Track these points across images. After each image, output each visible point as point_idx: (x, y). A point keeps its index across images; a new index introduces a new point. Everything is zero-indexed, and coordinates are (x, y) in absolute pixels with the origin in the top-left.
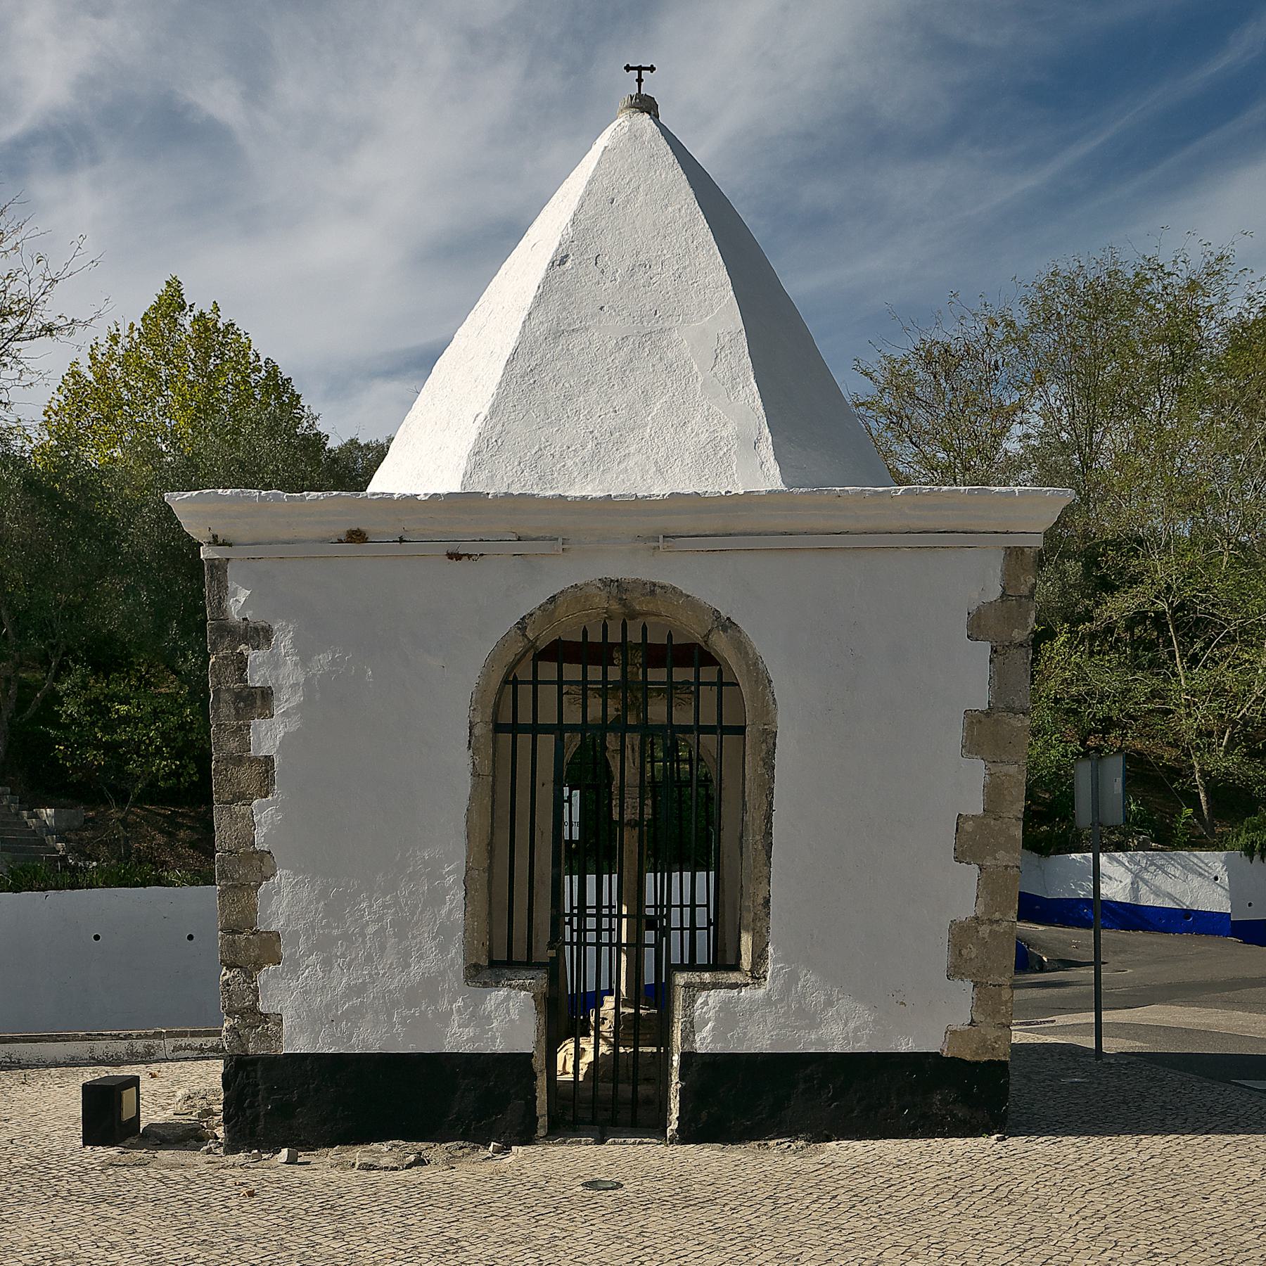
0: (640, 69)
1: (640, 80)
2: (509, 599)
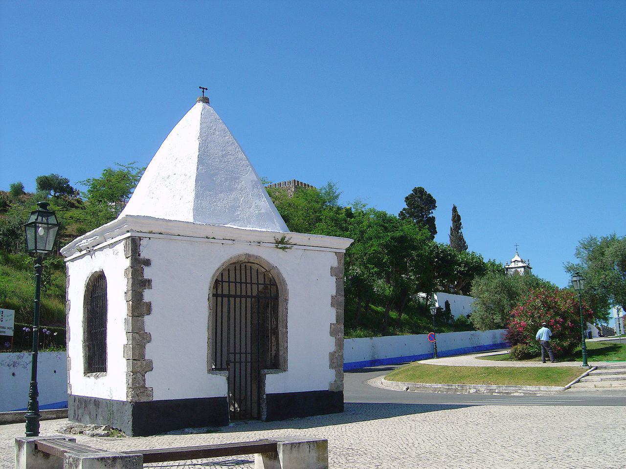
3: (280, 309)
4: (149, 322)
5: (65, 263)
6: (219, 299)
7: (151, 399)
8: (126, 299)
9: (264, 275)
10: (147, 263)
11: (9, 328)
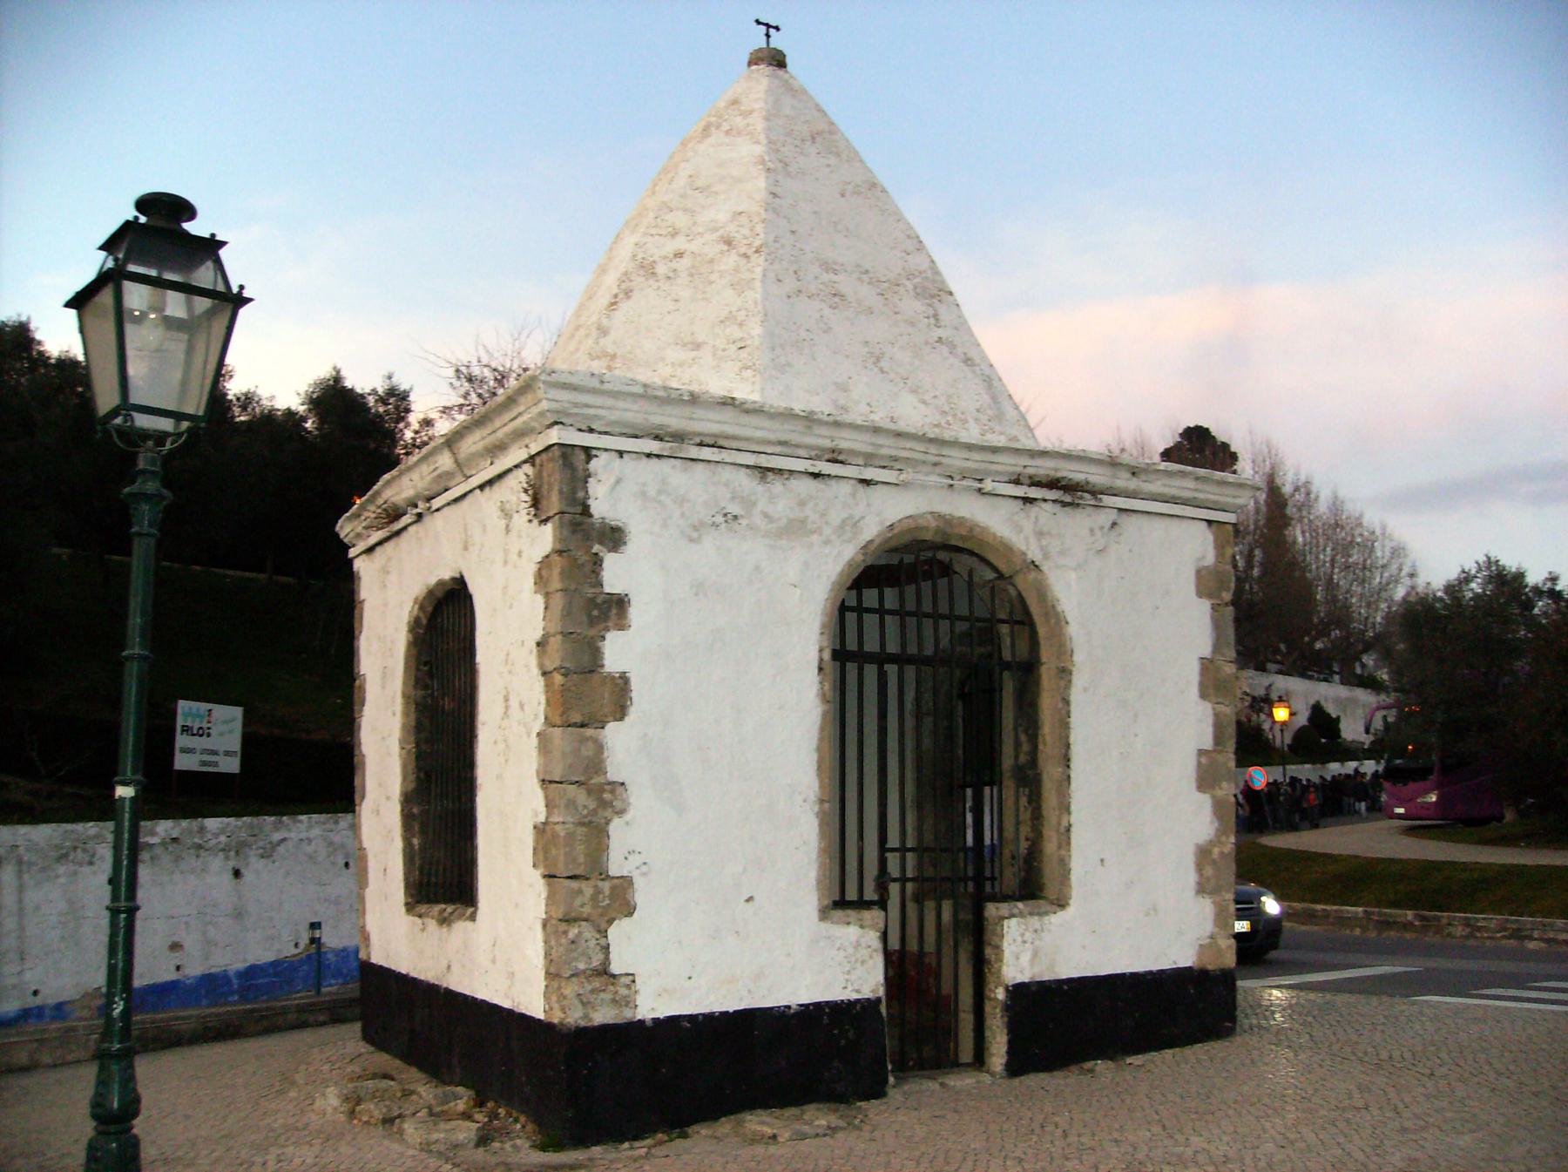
3: (1047, 702)
4: (620, 742)
5: (351, 560)
6: (852, 668)
7: (627, 1015)
8: (541, 666)
9: (993, 588)
10: (614, 537)
11: (227, 753)
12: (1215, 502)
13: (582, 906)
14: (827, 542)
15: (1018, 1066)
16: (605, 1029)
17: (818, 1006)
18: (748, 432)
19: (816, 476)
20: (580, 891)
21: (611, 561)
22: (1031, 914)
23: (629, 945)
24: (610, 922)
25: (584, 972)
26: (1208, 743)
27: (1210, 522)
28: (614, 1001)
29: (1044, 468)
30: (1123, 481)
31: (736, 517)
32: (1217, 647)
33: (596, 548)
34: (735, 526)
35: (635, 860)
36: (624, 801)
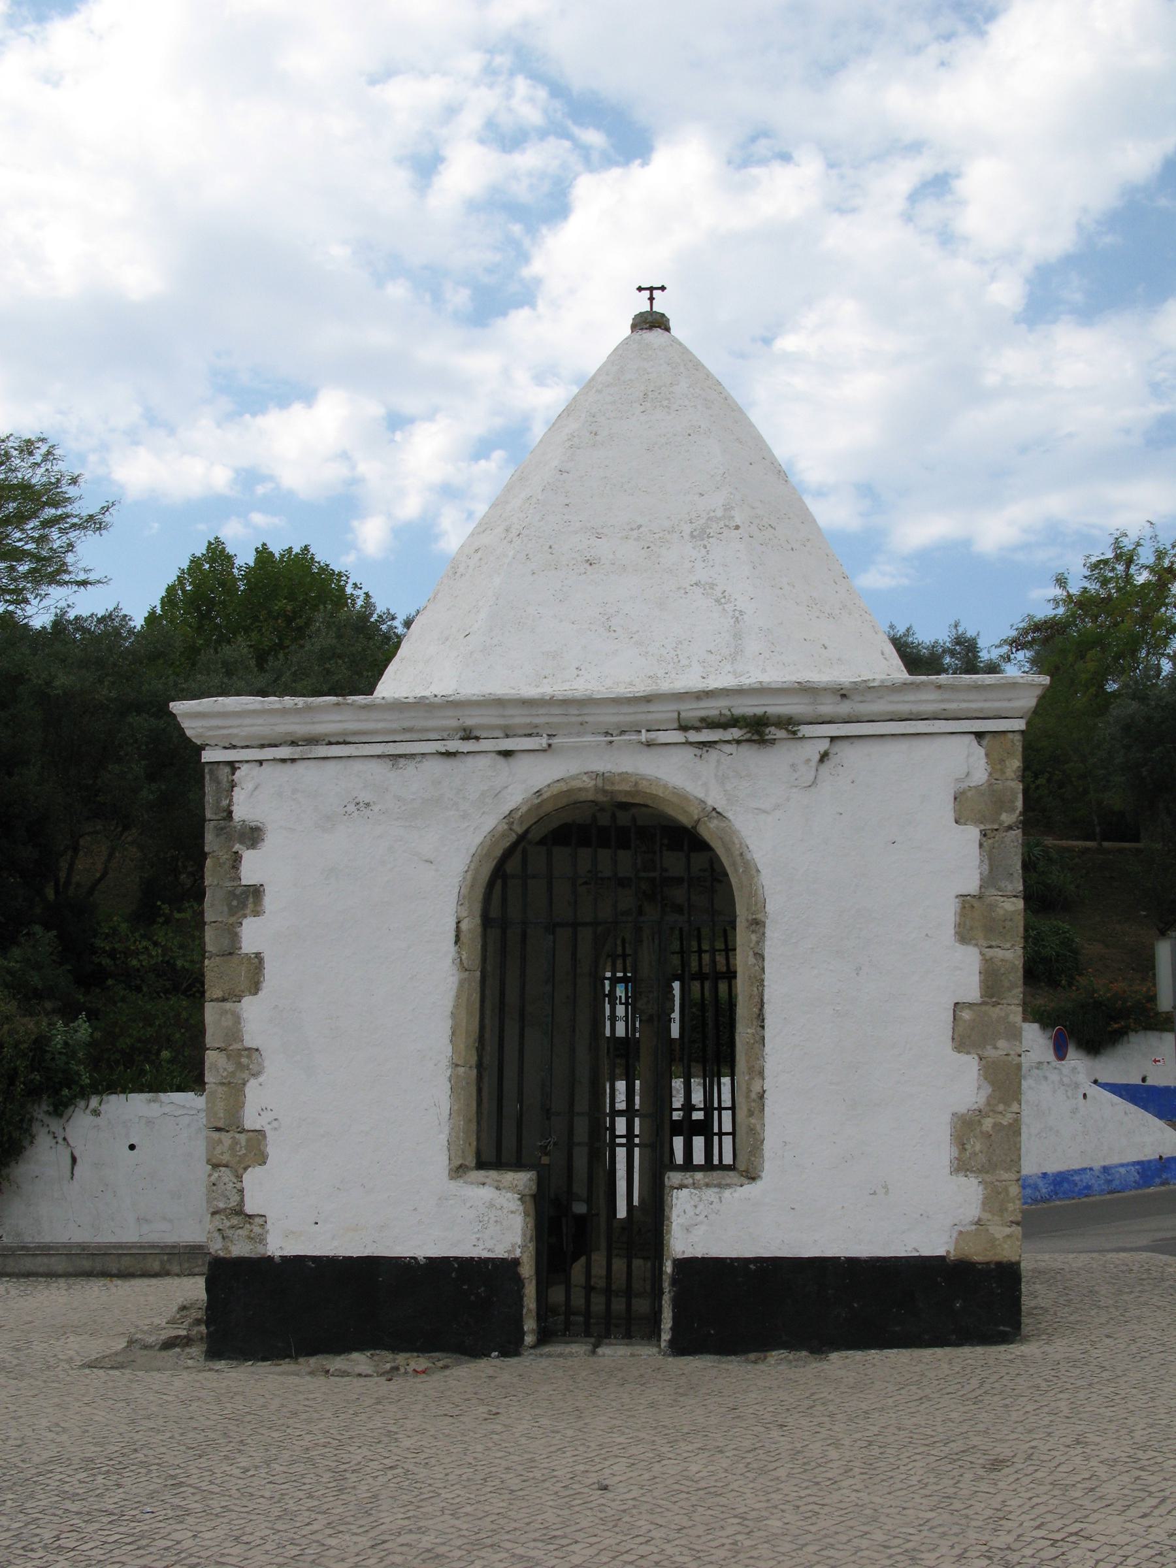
0: (651, 289)
1: (651, 299)
2: (502, 793)
12: (981, 710)
13: (222, 1154)
14: (465, 816)
15: (682, 1346)
16: (241, 1262)
17: (445, 1260)
18: (371, 726)
19: (448, 754)
20: (220, 1141)
21: (250, 859)
22: (707, 1185)
23: (261, 1190)
24: (245, 1169)
25: (225, 1209)
26: (972, 991)
27: (979, 735)
28: (249, 1237)
29: (711, 708)
30: (827, 708)
31: (368, 805)
32: (989, 881)
33: (237, 847)
34: (368, 812)
35: (267, 1116)
36: (260, 1064)
